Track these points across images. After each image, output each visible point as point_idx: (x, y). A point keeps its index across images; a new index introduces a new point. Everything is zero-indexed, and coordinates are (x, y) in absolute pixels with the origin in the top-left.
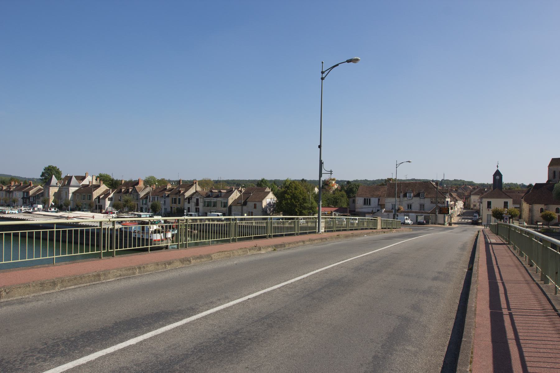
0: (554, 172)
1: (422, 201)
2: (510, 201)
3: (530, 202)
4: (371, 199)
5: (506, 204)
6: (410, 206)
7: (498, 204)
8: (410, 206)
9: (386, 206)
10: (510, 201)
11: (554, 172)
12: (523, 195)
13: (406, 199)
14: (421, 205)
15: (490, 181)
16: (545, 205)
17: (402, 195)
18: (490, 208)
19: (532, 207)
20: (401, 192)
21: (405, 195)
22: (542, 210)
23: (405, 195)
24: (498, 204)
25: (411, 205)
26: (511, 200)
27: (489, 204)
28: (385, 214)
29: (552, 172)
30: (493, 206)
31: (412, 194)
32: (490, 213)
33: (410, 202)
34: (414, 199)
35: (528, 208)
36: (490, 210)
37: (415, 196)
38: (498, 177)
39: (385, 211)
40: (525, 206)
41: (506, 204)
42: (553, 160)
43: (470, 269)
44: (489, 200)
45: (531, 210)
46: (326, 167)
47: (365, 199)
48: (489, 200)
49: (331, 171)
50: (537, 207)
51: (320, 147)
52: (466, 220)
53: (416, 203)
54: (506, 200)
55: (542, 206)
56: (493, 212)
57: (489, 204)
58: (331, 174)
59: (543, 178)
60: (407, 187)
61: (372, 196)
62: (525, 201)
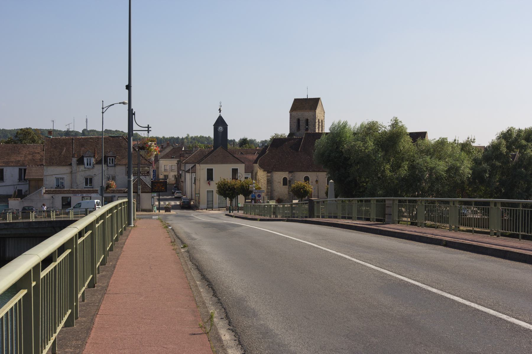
0: (299, 120)
1: (111, 171)
2: (241, 168)
3: (269, 169)
4: (5, 169)
5: (235, 171)
6: (89, 181)
7: (223, 172)
8: (89, 181)
9: (45, 182)
10: (241, 168)
11: (299, 120)
12: (255, 156)
13: (82, 167)
14: (86, 179)
15: (210, 133)
16: (290, 172)
17: (74, 160)
18: (212, 180)
19: (271, 176)
20: (73, 157)
21: (80, 162)
22: (285, 180)
23: (80, 162)
24: (223, 172)
25: (91, 180)
26: (243, 166)
27: (210, 173)
28: (47, 196)
29: (296, 121)
30: (217, 178)
31: (93, 160)
32: (214, 187)
33: (89, 173)
34: (98, 167)
35: (266, 179)
36: (211, 182)
37: (99, 162)
38: (220, 129)
39: (47, 192)
40: (262, 175)
41: (235, 171)
42: (296, 101)
43: (199, 268)
44: (210, 166)
45: (270, 182)
46: (140, 121)
47: (20, 170)
48: (210, 166)
49: (148, 127)
50: (279, 176)
51: (128, 87)
52: (167, 203)
53: (99, 173)
54: (235, 166)
55: (285, 174)
56: (219, 187)
57: (210, 173)
58: (148, 131)
59: (284, 129)
60: (83, 146)
61: (7, 164)
62: (262, 166)
